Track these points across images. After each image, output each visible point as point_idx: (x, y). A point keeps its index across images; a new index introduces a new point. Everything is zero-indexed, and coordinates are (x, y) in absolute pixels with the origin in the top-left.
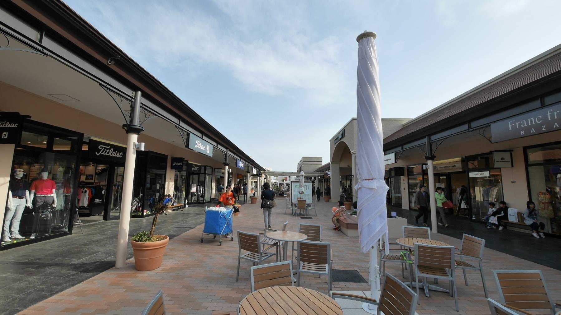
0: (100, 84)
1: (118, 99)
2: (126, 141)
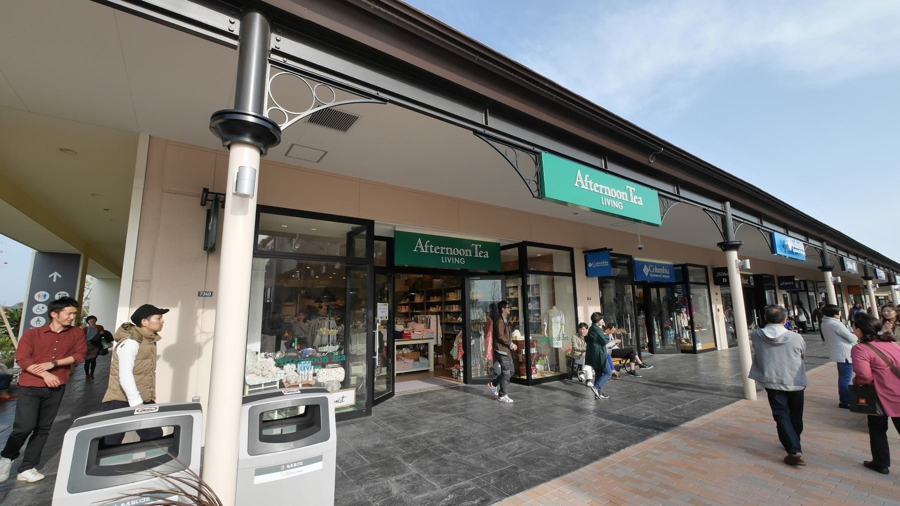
0: (704, 210)
1: (510, 152)
2: (725, 260)
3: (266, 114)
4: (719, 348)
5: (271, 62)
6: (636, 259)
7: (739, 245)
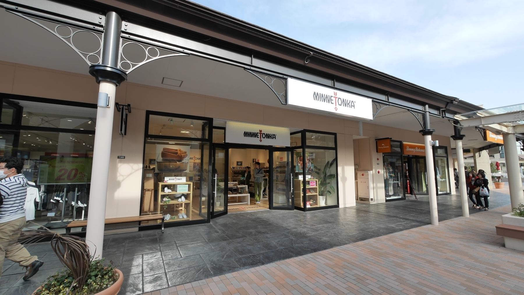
2: (423, 141)
3: (119, 66)
4: (341, 206)
5: (122, 37)
6: (404, 143)
7: (432, 132)
